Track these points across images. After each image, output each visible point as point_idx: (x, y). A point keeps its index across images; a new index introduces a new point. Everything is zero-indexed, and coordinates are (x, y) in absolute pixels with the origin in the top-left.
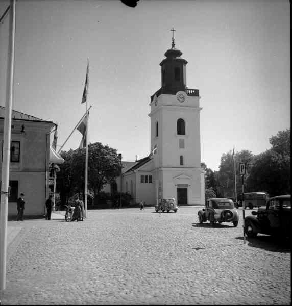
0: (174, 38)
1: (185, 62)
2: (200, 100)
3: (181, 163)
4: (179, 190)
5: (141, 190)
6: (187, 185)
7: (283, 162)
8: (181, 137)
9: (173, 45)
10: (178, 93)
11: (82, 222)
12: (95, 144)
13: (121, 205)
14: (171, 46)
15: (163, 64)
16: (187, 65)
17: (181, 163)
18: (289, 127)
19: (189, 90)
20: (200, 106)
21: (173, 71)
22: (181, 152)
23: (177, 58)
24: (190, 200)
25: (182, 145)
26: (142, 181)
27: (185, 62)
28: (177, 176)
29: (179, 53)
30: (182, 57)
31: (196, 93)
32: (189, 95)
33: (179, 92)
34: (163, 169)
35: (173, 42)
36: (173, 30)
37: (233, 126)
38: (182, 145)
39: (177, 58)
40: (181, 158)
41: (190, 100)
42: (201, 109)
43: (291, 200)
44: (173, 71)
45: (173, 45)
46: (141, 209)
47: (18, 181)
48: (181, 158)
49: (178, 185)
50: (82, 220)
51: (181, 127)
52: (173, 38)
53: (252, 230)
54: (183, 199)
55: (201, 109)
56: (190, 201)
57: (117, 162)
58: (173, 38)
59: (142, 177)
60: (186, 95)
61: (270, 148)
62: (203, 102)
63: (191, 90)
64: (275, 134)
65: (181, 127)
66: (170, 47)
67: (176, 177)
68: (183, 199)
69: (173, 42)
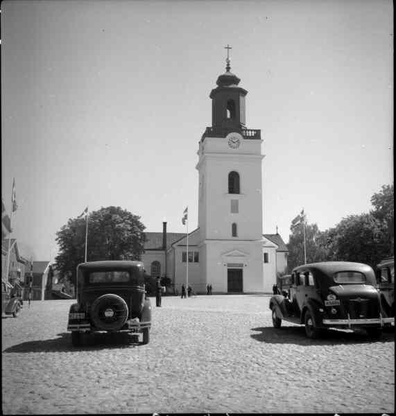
0: (230, 59)
1: (244, 93)
2: (262, 145)
3: (234, 234)
4: (230, 272)
5: (183, 273)
6: (242, 265)
7: (381, 230)
8: (234, 197)
9: (228, 69)
10: (230, 135)
11: (143, 347)
12: (108, 208)
13: (46, 270)
14: (226, 70)
15: (214, 94)
16: (247, 97)
17: (234, 234)
18: (390, 181)
19: (249, 130)
20: (263, 153)
21: (227, 100)
22: (234, 218)
23: (232, 86)
24: (247, 285)
25: (235, 208)
26: (184, 260)
27: (244, 93)
28: (228, 252)
29: (236, 81)
30: (240, 85)
31: (257, 135)
32: (246, 137)
33: (234, 133)
34: (206, 242)
35: (228, 65)
36: (228, 48)
37: (317, 182)
38: (235, 208)
39: (232, 86)
40: (234, 226)
41: (246, 145)
42: (264, 156)
43: (388, 281)
44: (227, 100)
45: (228, 69)
46: (182, 298)
47: (241, 271)
48: (234, 226)
49: (229, 265)
50: (145, 341)
51: (234, 183)
52: (228, 59)
53: (312, 326)
54: (235, 283)
55: (264, 156)
56: (245, 289)
57: (135, 233)
58: (228, 59)
59: (184, 255)
60: (242, 138)
61: (367, 212)
62: (267, 145)
63: (252, 131)
64: (378, 190)
65: (234, 183)
66: (224, 72)
67: (225, 253)
68: (235, 283)
69: (228, 65)
